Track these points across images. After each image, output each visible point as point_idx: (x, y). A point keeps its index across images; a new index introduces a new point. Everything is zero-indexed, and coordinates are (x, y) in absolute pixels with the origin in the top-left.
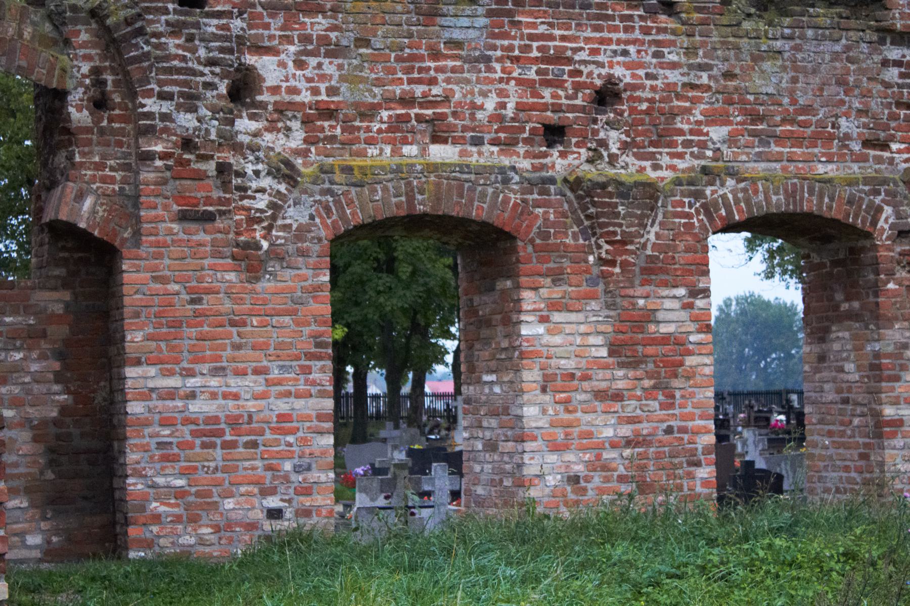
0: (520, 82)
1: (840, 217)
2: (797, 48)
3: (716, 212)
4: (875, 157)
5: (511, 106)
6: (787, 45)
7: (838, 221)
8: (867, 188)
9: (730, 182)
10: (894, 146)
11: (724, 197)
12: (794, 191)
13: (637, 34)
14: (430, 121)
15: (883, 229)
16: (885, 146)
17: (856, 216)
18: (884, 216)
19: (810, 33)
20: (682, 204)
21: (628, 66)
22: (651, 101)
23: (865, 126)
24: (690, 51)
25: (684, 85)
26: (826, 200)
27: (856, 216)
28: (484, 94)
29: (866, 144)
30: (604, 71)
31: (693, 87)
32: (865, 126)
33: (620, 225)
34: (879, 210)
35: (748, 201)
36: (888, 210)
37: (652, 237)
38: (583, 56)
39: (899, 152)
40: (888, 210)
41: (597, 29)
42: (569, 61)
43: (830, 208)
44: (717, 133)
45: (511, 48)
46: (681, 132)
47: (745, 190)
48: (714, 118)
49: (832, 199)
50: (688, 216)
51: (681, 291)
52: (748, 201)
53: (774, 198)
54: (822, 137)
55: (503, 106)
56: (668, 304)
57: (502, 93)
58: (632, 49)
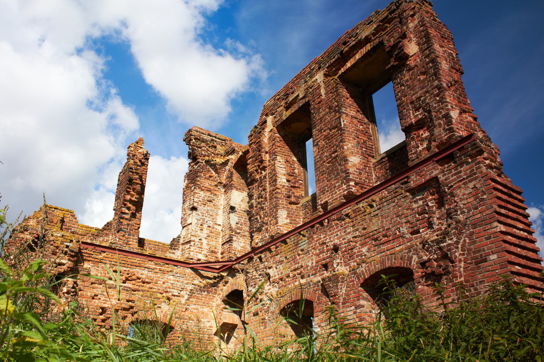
0: (315, 255)
1: (398, 265)
2: (382, 211)
3: (21, 285)
4: (415, 237)
5: (314, 262)
6: (379, 211)
7: (398, 267)
8: (406, 251)
9: (364, 265)
10: (421, 231)
11: (362, 271)
12: (383, 261)
13: (340, 228)
14: (300, 274)
15: (414, 265)
16: (419, 232)
17: (404, 264)
18: (413, 259)
19: (385, 203)
20: (351, 278)
21: (338, 239)
22: (345, 247)
23: (409, 227)
24: (353, 226)
25: (353, 238)
26: (393, 260)
27: (404, 264)
28: (308, 262)
29: (412, 233)
30: (332, 243)
31: (355, 237)
32: (409, 227)
33: (332, 290)
34: (412, 257)
35: (369, 270)
36: (415, 257)
37: (344, 292)
38: (328, 240)
39: (423, 232)
40: (415, 257)
41: (330, 231)
42: (325, 243)
43: (395, 263)
44: (364, 250)
45: (312, 246)
46: (355, 253)
47: (368, 266)
48: (363, 245)
49: (395, 259)
50: (353, 281)
51: (353, 308)
52: (369, 270)
53: (377, 266)
54: (396, 238)
55: (312, 263)
56: (349, 313)
57: (312, 260)
58: (339, 233)
